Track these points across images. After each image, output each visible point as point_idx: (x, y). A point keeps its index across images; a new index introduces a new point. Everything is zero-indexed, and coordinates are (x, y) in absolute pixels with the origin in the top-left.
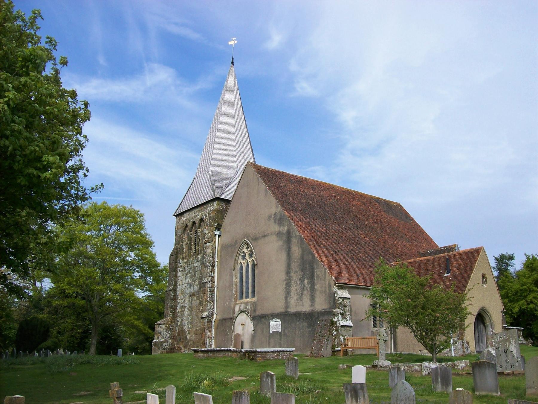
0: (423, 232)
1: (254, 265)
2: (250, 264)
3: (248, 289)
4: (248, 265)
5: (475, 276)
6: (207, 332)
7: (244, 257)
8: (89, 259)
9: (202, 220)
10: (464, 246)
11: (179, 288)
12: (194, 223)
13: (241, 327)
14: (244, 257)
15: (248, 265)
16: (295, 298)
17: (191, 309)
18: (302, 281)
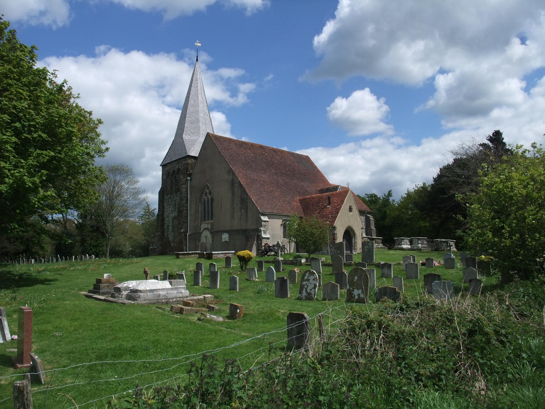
1: (212, 198)
4: (208, 200)
7: (206, 194)
9: (179, 169)
12: (174, 171)
13: (205, 238)
15: (208, 200)
17: (173, 227)
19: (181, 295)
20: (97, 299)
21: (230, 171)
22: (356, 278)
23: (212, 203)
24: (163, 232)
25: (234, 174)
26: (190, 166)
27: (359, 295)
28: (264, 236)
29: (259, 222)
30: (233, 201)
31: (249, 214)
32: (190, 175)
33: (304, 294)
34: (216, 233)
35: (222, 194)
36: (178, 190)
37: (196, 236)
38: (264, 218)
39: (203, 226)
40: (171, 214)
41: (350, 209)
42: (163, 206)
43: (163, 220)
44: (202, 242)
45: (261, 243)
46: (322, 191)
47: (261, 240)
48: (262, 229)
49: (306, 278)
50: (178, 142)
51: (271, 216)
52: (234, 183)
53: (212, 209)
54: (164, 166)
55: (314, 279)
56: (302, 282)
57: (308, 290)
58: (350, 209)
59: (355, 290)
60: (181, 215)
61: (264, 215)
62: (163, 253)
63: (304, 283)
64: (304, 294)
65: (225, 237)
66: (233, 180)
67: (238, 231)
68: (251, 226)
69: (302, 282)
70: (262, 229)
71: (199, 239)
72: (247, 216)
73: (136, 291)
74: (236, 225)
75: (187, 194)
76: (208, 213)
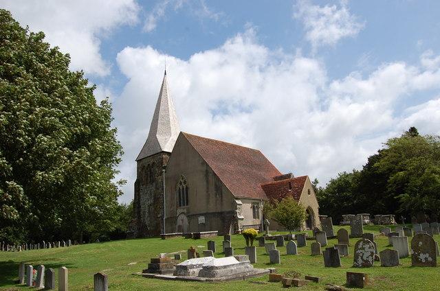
0: (273, 166)
1: (187, 188)
2: (185, 187)
3: (184, 201)
4: (183, 188)
5: (305, 190)
6: (161, 225)
7: (181, 183)
8: (209, 194)
9: (154, 163)
10: (296, 175)
11: (141, 202)
12: (149, 165)
13: (181, 221)
14: (181, 183)
15: (183, 188)
16: (341, 33)
17: (149, 212)
18: (216, 197)
19: (247, 270)
20: (156, 277)
21: (204, 163)
22: (421, 243)
23: (187, 191)
24: (139, 217)
25: (207, 165)
26: (164, 161)
27: (426, 258)
28: (239, 217)
29: (235, 206)
30: (208, 188)
31: (224, 198)
32: (165, 168)
33: (360, 261)
34: (192, 217)
35: (197, 184)
36: (153, 181)
37: (173, 219)
38: (238, 202)
39: (179, 211)
40: (146, 201)
41: (309, 193)
42: (139, 195)
43: (140, 207)
44: (178, 224)
45: (237, 223)
46: (276, 179)
47: (237, 221)
48: (237, 211)
49: (360, 247)
50: (152, 140)
51: (243, 199)
52: (208, 172)
53: (187, 197)
54: (139, 161)
55: (370, 248)
56: (355, 251)
57: (365, 258)
58: (309, 193)
59: (421, 255)
60: (157, 200)
61: (237, 199)
62: (140, 236)
63: (359, 251)
64: (360, 261)
65: (202, 219)
66: (207, 171)
67: (214, 214)
68: (226, 208)
69: (66, 265)
70: (237, 211)
71: (175, 222)
72: (222, 201)
73: (212, 268)
74: (212, 208)
75: (163, 184)
76: (184, 198)
